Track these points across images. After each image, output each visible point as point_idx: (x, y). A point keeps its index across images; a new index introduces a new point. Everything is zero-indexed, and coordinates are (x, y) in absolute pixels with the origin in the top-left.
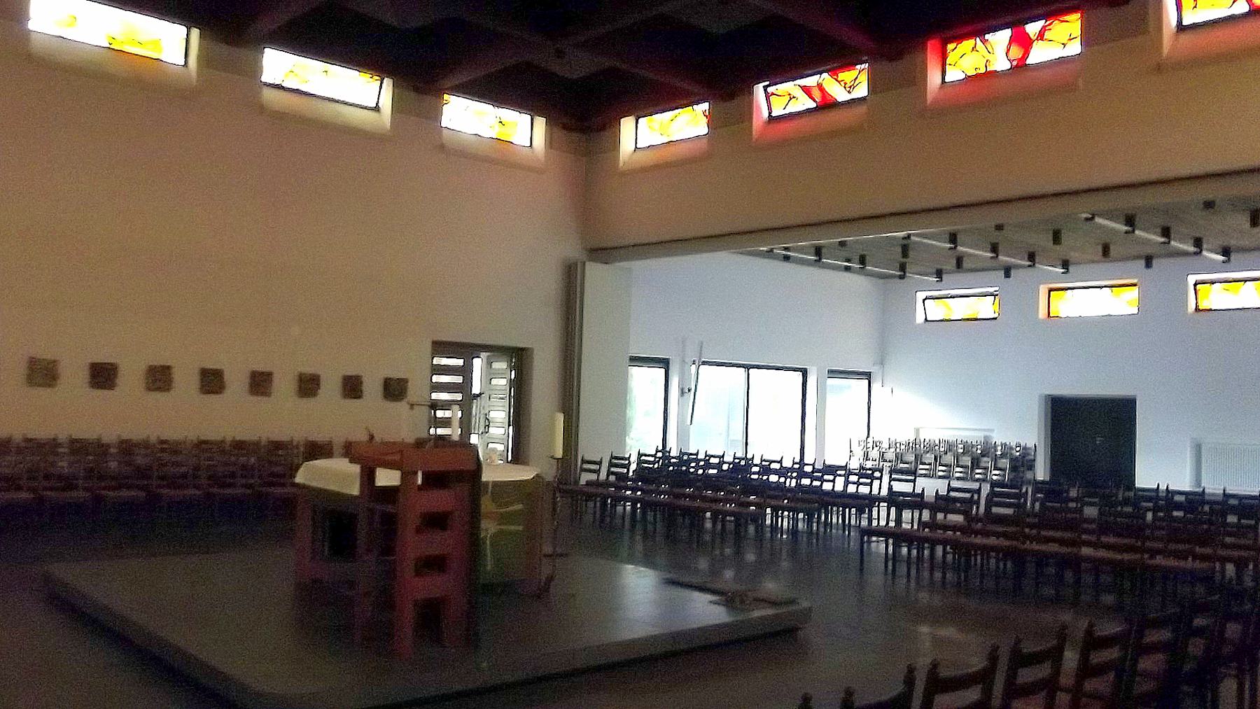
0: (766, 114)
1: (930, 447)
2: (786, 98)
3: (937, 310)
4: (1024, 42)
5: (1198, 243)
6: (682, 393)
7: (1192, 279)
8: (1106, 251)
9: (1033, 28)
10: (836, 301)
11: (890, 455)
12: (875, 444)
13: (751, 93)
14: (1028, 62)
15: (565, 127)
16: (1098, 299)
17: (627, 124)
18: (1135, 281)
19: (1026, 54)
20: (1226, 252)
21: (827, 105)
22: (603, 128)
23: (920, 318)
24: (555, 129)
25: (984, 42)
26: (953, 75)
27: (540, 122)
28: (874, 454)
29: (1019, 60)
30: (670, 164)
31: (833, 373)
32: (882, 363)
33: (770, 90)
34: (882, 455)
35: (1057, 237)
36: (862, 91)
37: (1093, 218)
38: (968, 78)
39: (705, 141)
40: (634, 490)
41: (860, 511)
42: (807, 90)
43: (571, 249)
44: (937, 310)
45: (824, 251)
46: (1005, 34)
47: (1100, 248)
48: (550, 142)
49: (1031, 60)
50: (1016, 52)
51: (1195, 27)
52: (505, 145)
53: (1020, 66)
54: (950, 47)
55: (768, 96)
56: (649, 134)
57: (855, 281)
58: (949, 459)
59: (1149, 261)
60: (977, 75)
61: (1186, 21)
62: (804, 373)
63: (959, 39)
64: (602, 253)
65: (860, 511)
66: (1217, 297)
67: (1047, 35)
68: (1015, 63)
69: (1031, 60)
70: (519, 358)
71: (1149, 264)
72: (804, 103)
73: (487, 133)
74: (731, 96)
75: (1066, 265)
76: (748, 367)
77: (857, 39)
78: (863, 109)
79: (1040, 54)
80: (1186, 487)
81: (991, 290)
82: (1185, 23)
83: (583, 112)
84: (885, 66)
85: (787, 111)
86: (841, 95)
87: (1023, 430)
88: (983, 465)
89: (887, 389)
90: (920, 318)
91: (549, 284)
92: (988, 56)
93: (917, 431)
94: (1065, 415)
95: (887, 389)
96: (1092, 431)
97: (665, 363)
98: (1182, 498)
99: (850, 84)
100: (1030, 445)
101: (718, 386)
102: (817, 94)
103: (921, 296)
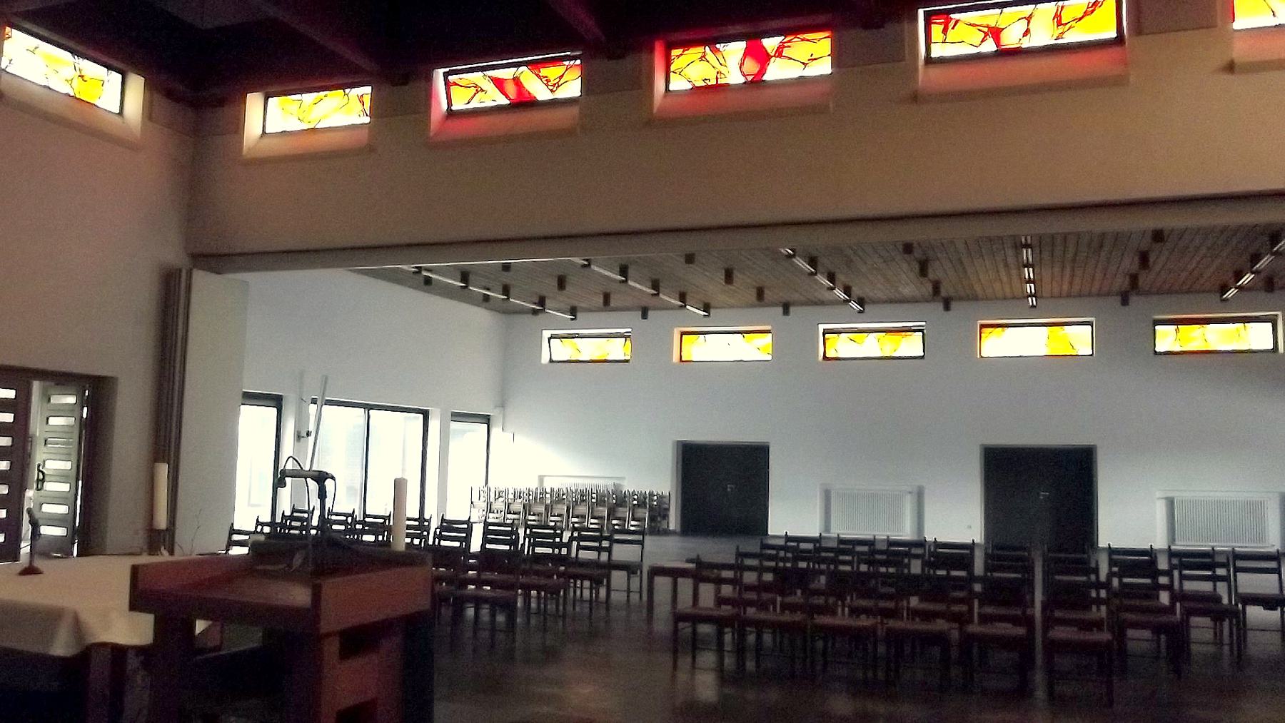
0: (445, 107)
1: (559, 497)
2: (469, 90)
3: (563, 350)
4: (763, 58)
5: (683, 297)
6: (299, 437)
7: (822, 327)
8: (607, 298)
9: (770, 44)
10: (459, 331)
11: (518, 506)
12: (498, 495)
13: (429, 79)
14: (766, 77)
15: (169, 94)
16: (730, 346)
17: (254, 102)
18: (768, 328)
19: (762, 71)
20: (707, 308)
21: (524, 103)
22: (221, 102)
23: (545, 359)
24: (157, 97)
25: (715, 51)
26: (678, 84)
27: (137, 84)
28: (499, 505)
29: (756, 75)
30: (312, 158)
31: (458, 417)
32: (502, 405)
33: (452, 78)
34: (508, 506)
35: (562, 283)
36: (572, 88)
37: (794, 256)
38: (695, 89)
39: (365, 133)
40: (479, 582)
41: (596, 582)
42: (499, 83)
43: (173, 255)
44: (563, 350)
45: (472, 277)
46: (740, 46)
47: (754, 292)
48: (149, 111)
49: (769, 76)
50: (751, 66)
51: (942, 61)
52: (86, 107)
53: (756, 82)
54: (675, 52)
55: (448, 85)
56: (277, 118)
57: (479, 317)
58: (582, 509)
59: (786, 308)
60: (708, 87)
61: (934, 54)
62: (426, 414)
63: (686, 45)
64: (216, 260)
65: (596, 582)
66: (841, 346)
67: (786, 52)
68: (750, 78)
69: (769, 76)
70: (96, 392)
71: (786, 312)
72: (494, 98)
73: (64, 89)
74: (404, 80)
75: (573, 311)
76: (368, 407)
77: (586, 22)
78: (575, 110)
79: (777, 71)
80: (814, 532)
81: (622, 331)
82: (933, 55)
83: (199, 74)
84: (603, 65)
85: (470, 106)
86: (540, 92)
87: (656, 478)
88: (619, 515)
89: (509, 435)
90: (545, 359)
91: (144, 297)
92: (722, 69)
93: (541, 479)
94: (694, 459)
95: (509, 435)
96: (722, 481)
97: (276, 401)
98: (810, 546)
99: (562, 81)
100: (658, 490)
101: (337, 433)
102: (511, 89)
103: (547, 334)
